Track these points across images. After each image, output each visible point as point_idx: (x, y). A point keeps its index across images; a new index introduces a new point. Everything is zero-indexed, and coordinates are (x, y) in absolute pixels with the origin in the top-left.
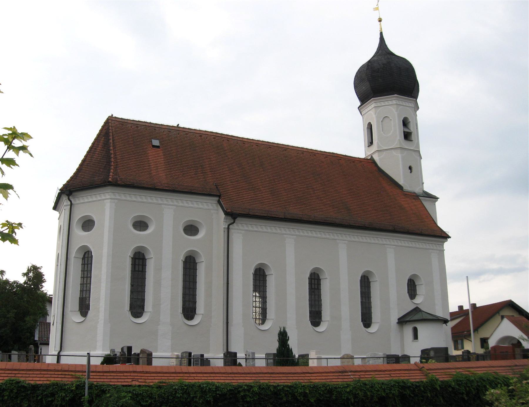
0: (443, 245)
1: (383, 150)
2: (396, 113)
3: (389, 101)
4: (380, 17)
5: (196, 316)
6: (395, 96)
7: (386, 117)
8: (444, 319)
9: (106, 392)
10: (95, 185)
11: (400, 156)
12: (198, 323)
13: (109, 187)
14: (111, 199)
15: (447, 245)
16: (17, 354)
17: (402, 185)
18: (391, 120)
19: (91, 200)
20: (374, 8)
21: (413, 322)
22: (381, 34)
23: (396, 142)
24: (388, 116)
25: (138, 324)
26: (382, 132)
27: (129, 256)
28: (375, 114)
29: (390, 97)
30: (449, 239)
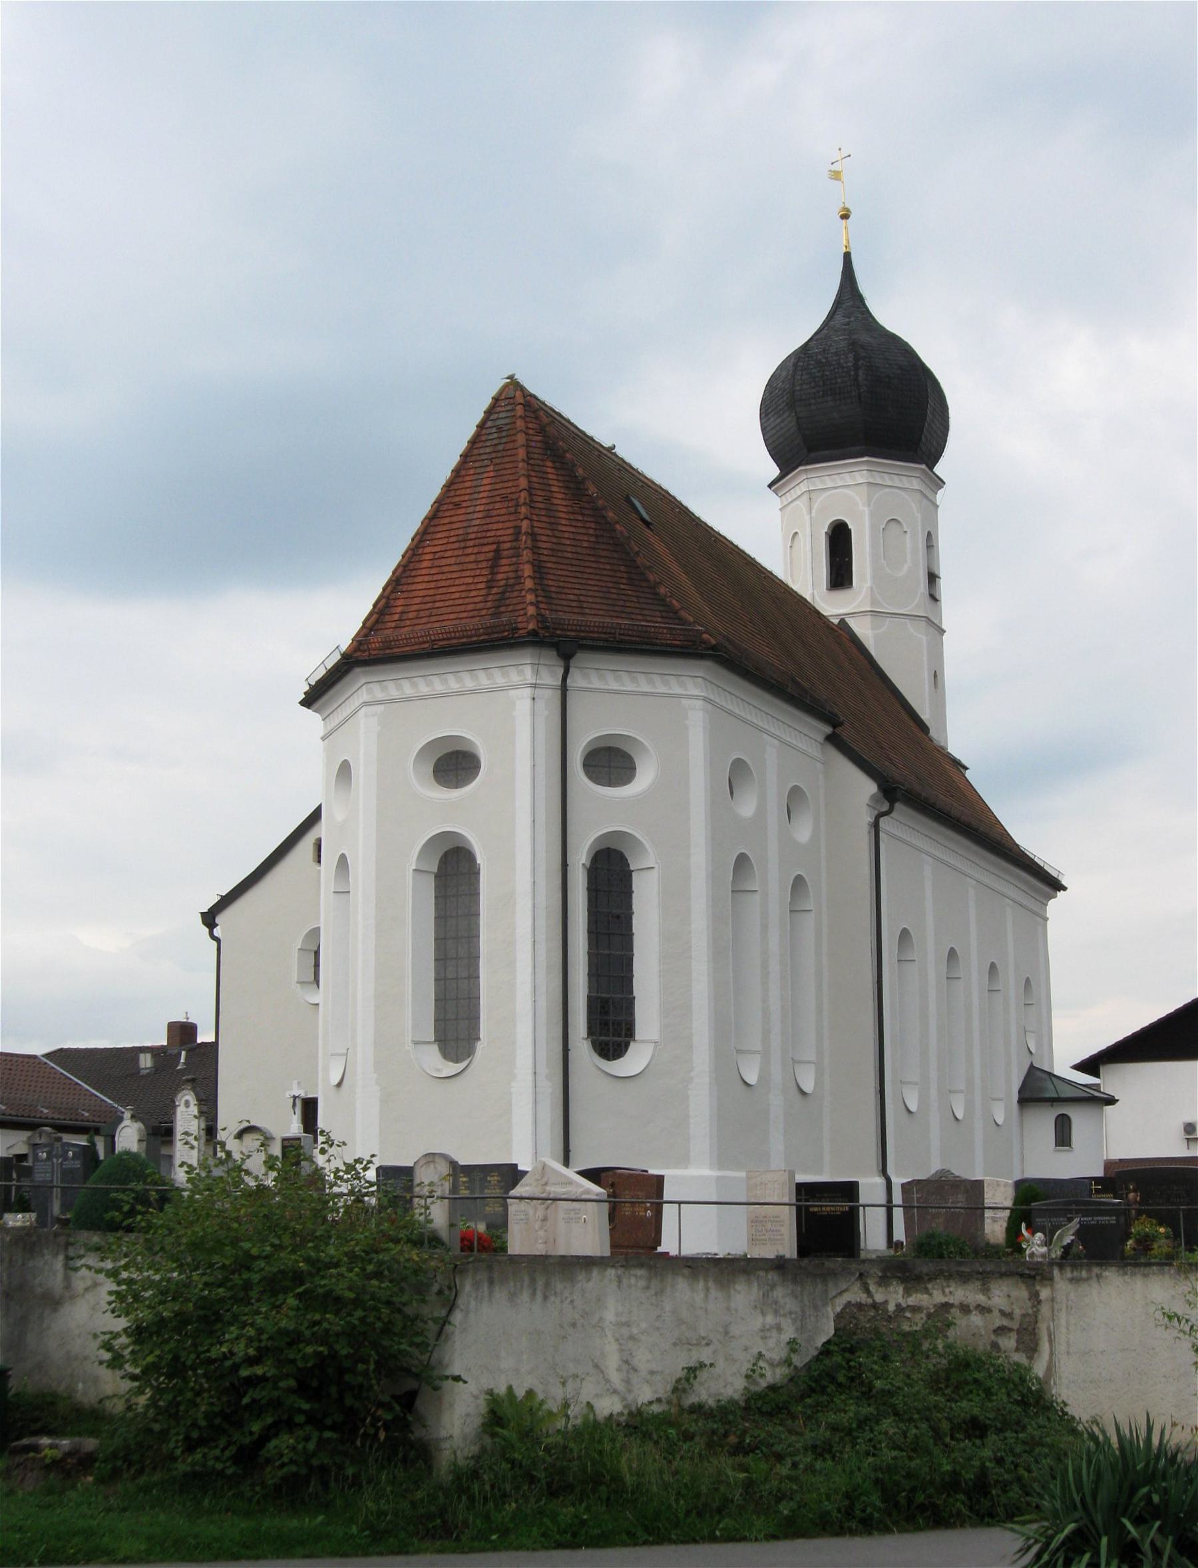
0: (1047, 905)
1: (884, 613)
2: (866, 509)
3: (904, 478)
4: (847, 206)
5: (632, 1045)
6: (920, 469)
7: (892, 520)
8: (1105, 1096)
9: (27, 1197)
10: (663, 645)
11: (925, 642)
12: (642, 1068)
13: (708, 663)
14: (705, 699)
15: (1056, 906)
16: (606, 1201)
17: (928, 723)
18: (906, 532)
19: (662, 689)
20: (830, 171)
21: (878, 1069)
22: (847, 257)
23: (918, 599)
24: (900, 519)
25: (621, 1080)
26: (883, 561)
27: (583, 864)
28: (869, 501)
29: (874, 462)
30: (1060, 894)
